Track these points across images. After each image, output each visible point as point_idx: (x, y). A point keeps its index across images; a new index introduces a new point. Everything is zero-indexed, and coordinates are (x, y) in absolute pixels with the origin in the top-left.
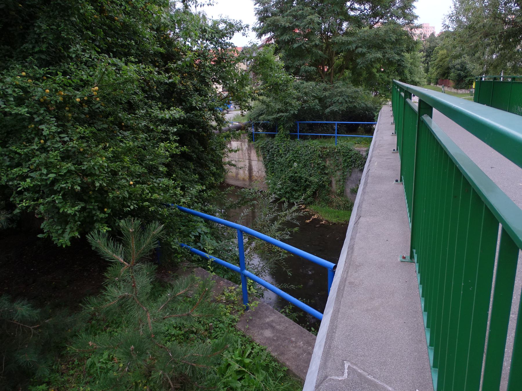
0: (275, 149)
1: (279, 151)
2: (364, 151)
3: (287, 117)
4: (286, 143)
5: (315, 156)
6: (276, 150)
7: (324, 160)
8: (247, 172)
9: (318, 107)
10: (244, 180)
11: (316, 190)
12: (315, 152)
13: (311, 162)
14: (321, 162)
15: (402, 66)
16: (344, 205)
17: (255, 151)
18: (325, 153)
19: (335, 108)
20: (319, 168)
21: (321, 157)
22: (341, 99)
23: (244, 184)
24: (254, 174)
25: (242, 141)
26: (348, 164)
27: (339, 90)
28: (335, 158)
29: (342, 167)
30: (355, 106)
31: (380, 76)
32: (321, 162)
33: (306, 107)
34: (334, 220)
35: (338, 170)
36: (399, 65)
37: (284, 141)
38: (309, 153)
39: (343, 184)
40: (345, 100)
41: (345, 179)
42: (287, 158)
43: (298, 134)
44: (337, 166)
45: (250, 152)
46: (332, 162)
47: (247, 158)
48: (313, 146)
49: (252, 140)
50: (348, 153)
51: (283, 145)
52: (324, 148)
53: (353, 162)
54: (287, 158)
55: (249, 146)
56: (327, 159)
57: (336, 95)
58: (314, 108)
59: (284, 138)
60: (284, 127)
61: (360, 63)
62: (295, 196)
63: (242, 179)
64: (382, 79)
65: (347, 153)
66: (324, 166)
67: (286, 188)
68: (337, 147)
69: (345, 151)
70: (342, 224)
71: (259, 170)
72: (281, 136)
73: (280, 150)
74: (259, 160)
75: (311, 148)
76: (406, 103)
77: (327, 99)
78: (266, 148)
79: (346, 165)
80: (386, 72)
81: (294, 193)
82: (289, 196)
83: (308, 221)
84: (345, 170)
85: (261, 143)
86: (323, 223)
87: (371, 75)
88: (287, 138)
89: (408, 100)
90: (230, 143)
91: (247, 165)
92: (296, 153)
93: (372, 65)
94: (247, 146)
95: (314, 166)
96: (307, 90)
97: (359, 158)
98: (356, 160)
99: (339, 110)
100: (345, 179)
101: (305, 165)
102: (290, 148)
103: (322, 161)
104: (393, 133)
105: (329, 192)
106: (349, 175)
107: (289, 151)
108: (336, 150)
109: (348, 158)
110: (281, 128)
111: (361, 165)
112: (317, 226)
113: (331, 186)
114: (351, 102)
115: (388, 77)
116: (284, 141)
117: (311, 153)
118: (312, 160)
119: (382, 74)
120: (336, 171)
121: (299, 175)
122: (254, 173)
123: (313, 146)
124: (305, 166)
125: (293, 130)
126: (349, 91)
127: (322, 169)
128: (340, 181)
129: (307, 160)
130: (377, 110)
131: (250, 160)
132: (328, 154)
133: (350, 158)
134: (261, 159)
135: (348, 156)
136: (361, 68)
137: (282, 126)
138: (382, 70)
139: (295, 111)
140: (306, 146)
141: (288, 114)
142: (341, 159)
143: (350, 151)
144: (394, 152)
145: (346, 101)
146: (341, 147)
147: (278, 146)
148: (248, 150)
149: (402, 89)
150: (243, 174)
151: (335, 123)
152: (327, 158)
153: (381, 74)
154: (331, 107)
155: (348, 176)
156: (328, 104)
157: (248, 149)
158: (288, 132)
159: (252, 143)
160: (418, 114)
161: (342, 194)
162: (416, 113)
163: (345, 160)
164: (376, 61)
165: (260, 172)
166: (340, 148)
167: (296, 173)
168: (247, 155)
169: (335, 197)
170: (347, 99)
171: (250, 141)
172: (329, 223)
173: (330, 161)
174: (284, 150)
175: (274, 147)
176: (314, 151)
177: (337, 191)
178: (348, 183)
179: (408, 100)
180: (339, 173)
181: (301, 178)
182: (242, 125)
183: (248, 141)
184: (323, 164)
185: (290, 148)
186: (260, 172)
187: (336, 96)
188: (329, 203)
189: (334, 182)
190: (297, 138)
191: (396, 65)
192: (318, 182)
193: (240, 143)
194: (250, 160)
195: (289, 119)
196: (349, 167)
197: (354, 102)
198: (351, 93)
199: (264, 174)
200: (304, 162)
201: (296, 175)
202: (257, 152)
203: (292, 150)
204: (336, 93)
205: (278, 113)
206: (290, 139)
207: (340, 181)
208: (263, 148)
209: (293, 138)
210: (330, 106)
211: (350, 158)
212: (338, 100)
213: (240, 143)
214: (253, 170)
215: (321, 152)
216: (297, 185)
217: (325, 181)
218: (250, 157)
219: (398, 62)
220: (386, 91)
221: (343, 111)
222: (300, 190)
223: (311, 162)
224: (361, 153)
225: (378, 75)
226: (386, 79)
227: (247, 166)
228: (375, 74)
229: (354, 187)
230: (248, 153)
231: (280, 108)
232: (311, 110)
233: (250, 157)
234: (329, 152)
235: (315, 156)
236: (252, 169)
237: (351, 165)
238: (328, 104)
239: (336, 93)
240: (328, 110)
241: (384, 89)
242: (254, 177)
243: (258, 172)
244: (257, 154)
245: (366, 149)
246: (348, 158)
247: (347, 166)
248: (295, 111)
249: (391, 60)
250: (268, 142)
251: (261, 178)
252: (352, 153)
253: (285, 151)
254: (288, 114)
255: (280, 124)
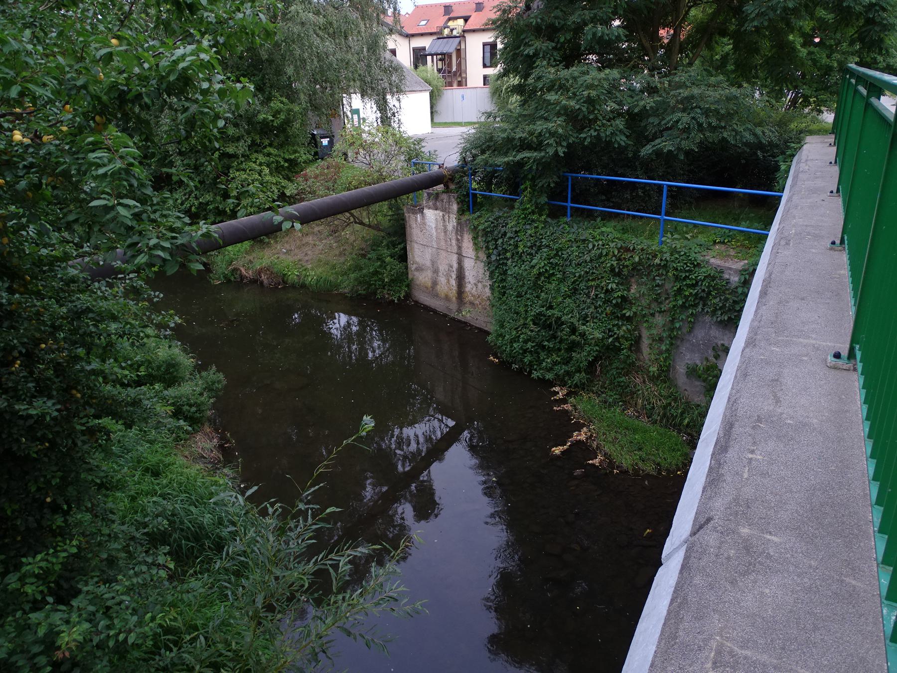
0: (510, 238)
1: (516, 246)
2: (736, 271)
3: (538, 161)
4: (536, 227)
5: (600, 270)
6: (512, 242)
7: (625, 282)
8: (453, 282)
9: (622, 140)
10: (447, 298)
11: (596, 359)
12: (603, 259)
13: (591, 283)
14: (614, 286)
15: (880, 23)
16: (665, 408)
17: (471, 237)
18: (627, 263)
19: (666, 144)
20: (607, 301)
21: (619, 274)
22: (686, 118)
23: (447, 307)
24: (467, 289)
25: (444, 210)
26: (687, 300)
27: (685, 93)
28: (654, 279)
29: (671, 305)
30: (724, 139)
31: (810, 53)
32: (614, 286)
33: (589, 140)
34: (626, 460)
35: (660, 312)
36: (870, 22)
37: (533, 221)
38: (588, 259)
39: (667, 350)
40: (698, 123)
41: (674, 339)
42: (533, 267)
43: (569, 204)
44: (656, 300)
45: (462, 236)
46: (643, 289)
47: (455, 249)
48: (600, 243)
49: (468, 210)
50: (690, 271)
51: (529, 232)
52: (627, 250)
53: (701, 298)
54: (533, 267)
55: (459, 223)
56: (633, 280)
57: (675, 106)
58: (610, 141)
59: (533, 213)
60: (533, 186)
61: (753, 15)
62: (544, 364)
63: (443, 295)
64: (815, 62)
65: (686, 271)
66: (622, 297)
67: (526, 342)
68: (661, 252)
69: (679, 265)
70: (648, 476)
71: (479, 282)
72: (526, 209)
73: (520, 244)
74: (477, 258)
75: (594, 246)
76: (868, 106)
77: (649, 116)
78: (492, 232)
79: (680, 302)
80: (824, 44)
81: (543, 355)
82: (530, 362)
83: (557, 450)
84: (677, 316)
85: (485, 219)
86: (596, 462)
87: (784, 51)
88: (541, 215)
89: (873, 100)
90: (422, 213)
91: (455, 266)
92: (556, 255)
93: (788, 24)
94: (455, 224)
95: (597, 295)
96: (593, 93)
97: (717, 289)
98: (709, 293)
99: (679, 149)
100: (676, 337)
101: (576, 289)
102: (544, 242)
103: (617, 284)
104: (833, 243)
105: (631, 368)
106: (685, 330)
107: (539, 248)
108: (657, 261)
109: (688, 286)
110: (526, 188)
111: (721, 308)
112: (578, 472)
113: (638, 350)
114: (713, 129)
115: (829, 57)
116: (533, 221)
117: (591, 261)
118: (593, 280)
119: (816, 50)
120: (653, 315)
121: (557, 313)
122: (469, 287)
123: (600, 243)
124: (575, 291)
125: (558, 193)
126: (713, 95)
127: (617, 305)
128: (661, 340)
129: (580, 276)
130: (789, 152)
131: (460, 255)
132: (635, 269)
133: (693, 286)
134: (483, 256)
135: (688, 282)
136: (758, 29)
137: (528, 183)
138: (817, 40)
139: (559, 149)
140: (584, 241)
141: (543, 154)
142: (671, 286)
143: (695, 266)
144: (840, 362)
145: (700, 125)
146: (672, 255)
147: (516, 232)
148: (457, 234)
149: (862, 79)
150: (447, 285)
151: (660, 187)
152: (633, 276)
153: (812, 49)
154: (657, 141)
155: (685, 330)
156: (651, 130)
157: (457, 230)
158: (543, 199)
159: (467, 216)
160: (893, 125)
161: (664, 375)
162: (890, 125)
163: (680, 291)
164: (803, 9)
165: (480, 285)
166: (667, 256)
167: (551, 307)
168: (454, 242)
169: (644, 382)
170: (702, 119)
171: (461, 212)
172: (612, 464)
173: (638, 284)
174: (529, 244)
175: (509, 235)
176: (601, 256)
177: (651, 369)
178: (683, 349)
179: (873, 100)
180: (659, 320)
181: (559, 322)
182: (445, 172)
183: (458, 212)
184: (619, 294)
185: (544, 242)
186: (480, 285)
187: (674, 110)
188: (626, 396)
189: (645, 342)
190: (565, 215)
191: (862, 22)
192: (603, 339)
193: (441, 214)
194: (460, 255)
195: (545, 167)
196: (687, 308)
197: (725, 128)
198: (717, 102)
199: (488, 292)
200: (574, 282)
201: (549, 313)
202: (475, 238)
203: (548, 246)
204: (673, 102)
205: (518, 151)
206: (548, 216)
207: (661, 340)
208: (486, 233)
209: (556, 213)
210: (655, 137)
211: (693, 286)
212: (677, 122)
213: (441, 214)
214: (467, 281)
215: (619, 259)
216: (554, 337)
217: (623, 336)
218: (460, 248)
219: (866, 12)
220: (821, 90)
221: (688, 153)
222: (559, 350)
223: (591, 283)
224: (726, 276)
225: (803, 52)
226: (824, 61)
227: (454, 269)
228: (794, 49)
229: (698, 362)
230: (458, 240)
231: (525, 139)
232: (603, 146)
233: (460, 248)
234: (640, 263)
235: (600, 270)
236: (464, 278)
237: (696, 305)
238: (651, 130)
239: (673, 102)
240: (647, 150)
241: (815, 85)
242: (468, 296)
243: (475, 284)
244: (475, 244)
245: (739, 265)
246: (688, 286)
247: (683, 306)
248: (559, 149)
249: (849, 7)
250: (497, 219)
251: (482, 299)
252: (701, 273)
253: (531, 247)
254: (543, 154)
255: (525, 178)
